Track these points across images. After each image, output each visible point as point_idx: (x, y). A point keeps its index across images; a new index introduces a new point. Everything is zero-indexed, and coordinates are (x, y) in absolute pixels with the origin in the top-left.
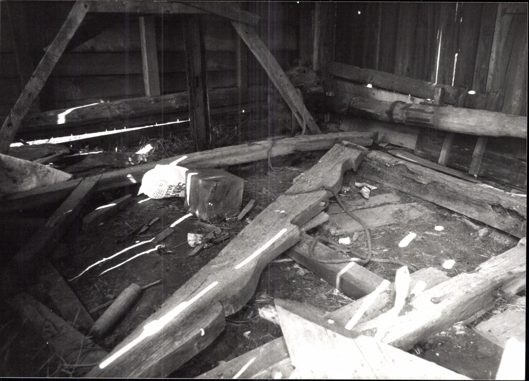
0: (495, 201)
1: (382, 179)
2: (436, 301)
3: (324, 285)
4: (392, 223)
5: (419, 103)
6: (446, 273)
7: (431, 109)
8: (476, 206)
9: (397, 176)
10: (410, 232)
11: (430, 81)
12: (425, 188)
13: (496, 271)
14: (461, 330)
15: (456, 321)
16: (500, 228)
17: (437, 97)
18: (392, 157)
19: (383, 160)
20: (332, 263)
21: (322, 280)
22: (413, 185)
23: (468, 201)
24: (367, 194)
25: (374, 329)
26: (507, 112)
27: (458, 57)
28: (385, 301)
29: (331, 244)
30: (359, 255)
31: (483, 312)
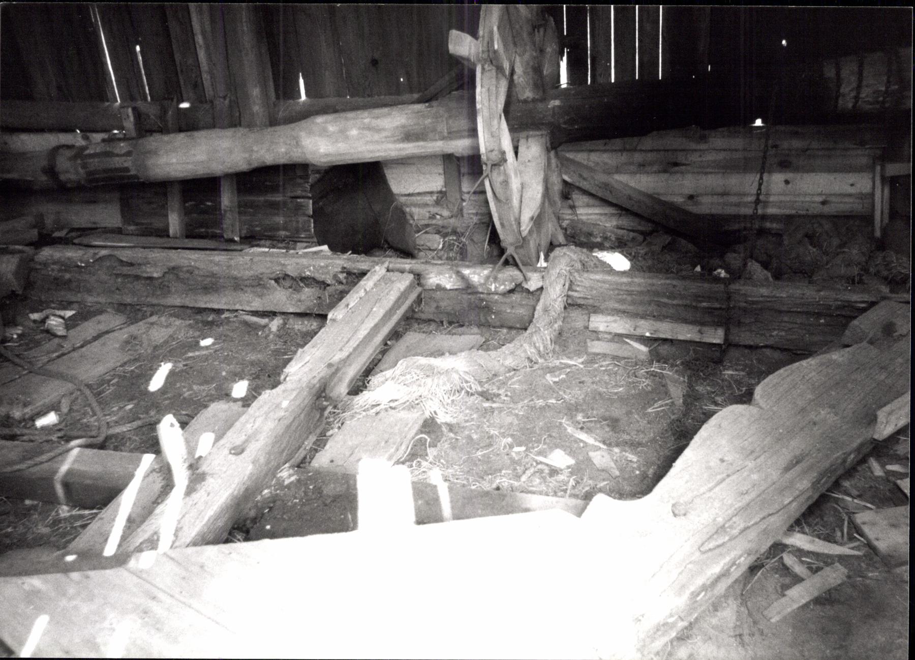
0: (277, 270)
1: (79, 292)
2: (238, 451)
3: (36, 510)
4: (125, 360)
5: (99, 140)
6: (240, 403)
7: (123, 147)
8: (253, 289)
9: (104, 277)
10: (162, 364)
11: (108, 101)
12: (161, 283)
13: (311, 370)
14: (290, 476)
15: (278, 467)
16: (298, 311)
17: (130, 122)
18: (84, 248)
19: (69, 259)
20: (36, 465)
21: (28, 502)
22: (139, 285)
23: (238, 285)
24: (61, 328)
25: (153, 536)
26: (250, 126)
27: (142, 51)
28: (158, 486)
29: (23, 435)
30: (83, 434)
31: (313, 438)
